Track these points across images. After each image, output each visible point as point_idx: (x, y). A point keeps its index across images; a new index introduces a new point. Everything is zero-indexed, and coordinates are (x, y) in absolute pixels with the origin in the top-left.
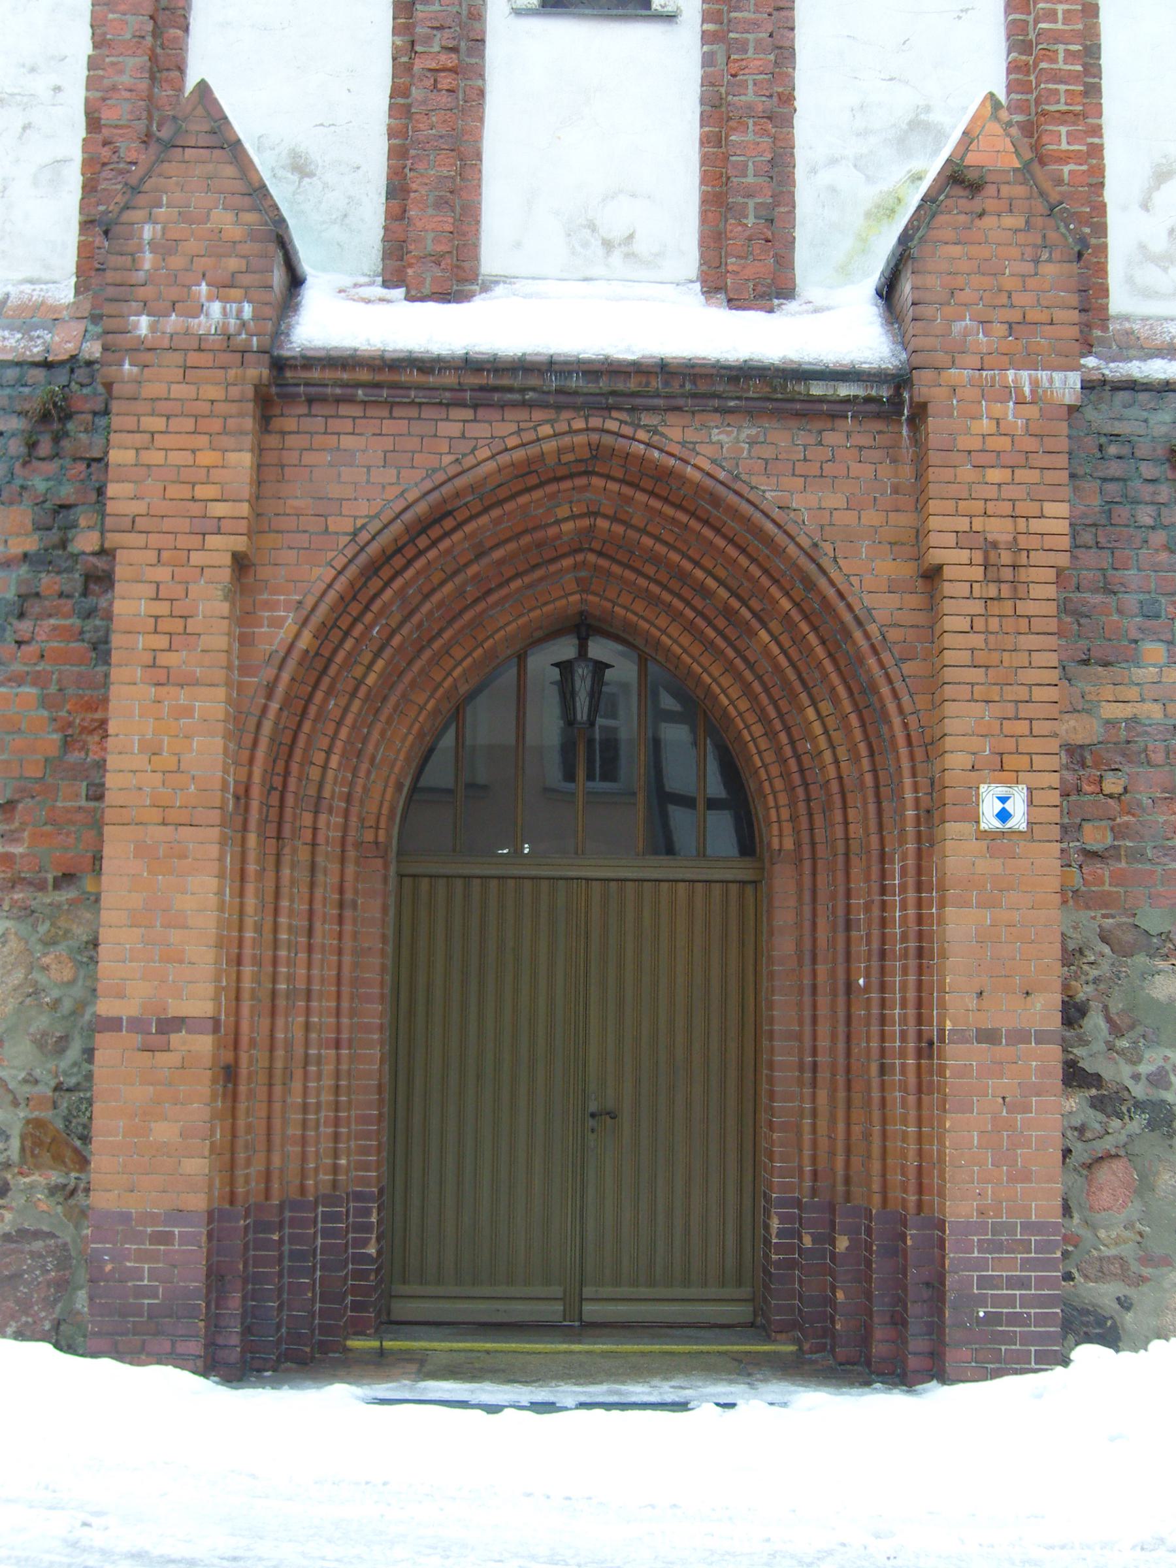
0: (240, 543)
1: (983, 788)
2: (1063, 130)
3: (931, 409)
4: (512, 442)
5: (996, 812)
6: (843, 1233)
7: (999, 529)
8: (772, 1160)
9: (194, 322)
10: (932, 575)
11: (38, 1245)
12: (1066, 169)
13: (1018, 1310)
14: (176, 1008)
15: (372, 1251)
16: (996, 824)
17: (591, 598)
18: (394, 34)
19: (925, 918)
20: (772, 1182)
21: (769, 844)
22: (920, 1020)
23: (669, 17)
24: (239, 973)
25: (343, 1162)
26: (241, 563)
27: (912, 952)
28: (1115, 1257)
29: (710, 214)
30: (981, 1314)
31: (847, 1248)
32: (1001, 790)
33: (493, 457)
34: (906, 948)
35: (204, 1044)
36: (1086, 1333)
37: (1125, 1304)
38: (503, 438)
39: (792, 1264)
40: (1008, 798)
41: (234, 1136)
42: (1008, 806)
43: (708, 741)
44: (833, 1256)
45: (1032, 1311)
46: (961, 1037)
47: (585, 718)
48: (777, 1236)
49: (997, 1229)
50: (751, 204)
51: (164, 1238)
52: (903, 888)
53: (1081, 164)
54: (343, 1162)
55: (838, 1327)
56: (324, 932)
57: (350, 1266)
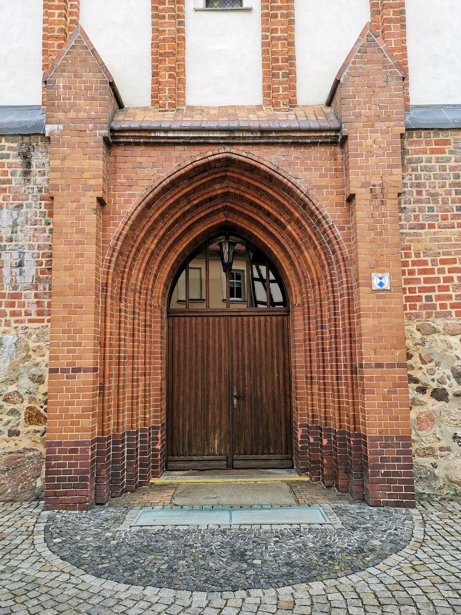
0: (100, 194)
1: (373, 274)
3: (349, 138)
6: (325, 438)
7: (376, 180)
8: (297, 411)
11: (31, 454)
13: (397, 470)
14: (79, 363)
18: (152, 18)
20: (297, 418)
21: (292, 302)
22: (351, 361)
23: (249, 10)
24: (104, 350)
26: (101, 202)
29: (266, 79)
30: (383, 472)
31: (327, 444)
32: (380, 275)
33: (191, 163)
34: (345, 334)
35: (90, 377)
36: (420, 477)
37: (435, 466)
38: (194, 157)
40: (383, 278)
42: (383, 281)
44: (321, 446)
45: (402, 471)
47: (227, 261)
49: (387, 438)
52: (343, 313)
53: (218, 451)
55: (325, 473)
56: (140, 336)
57: (151, 453)
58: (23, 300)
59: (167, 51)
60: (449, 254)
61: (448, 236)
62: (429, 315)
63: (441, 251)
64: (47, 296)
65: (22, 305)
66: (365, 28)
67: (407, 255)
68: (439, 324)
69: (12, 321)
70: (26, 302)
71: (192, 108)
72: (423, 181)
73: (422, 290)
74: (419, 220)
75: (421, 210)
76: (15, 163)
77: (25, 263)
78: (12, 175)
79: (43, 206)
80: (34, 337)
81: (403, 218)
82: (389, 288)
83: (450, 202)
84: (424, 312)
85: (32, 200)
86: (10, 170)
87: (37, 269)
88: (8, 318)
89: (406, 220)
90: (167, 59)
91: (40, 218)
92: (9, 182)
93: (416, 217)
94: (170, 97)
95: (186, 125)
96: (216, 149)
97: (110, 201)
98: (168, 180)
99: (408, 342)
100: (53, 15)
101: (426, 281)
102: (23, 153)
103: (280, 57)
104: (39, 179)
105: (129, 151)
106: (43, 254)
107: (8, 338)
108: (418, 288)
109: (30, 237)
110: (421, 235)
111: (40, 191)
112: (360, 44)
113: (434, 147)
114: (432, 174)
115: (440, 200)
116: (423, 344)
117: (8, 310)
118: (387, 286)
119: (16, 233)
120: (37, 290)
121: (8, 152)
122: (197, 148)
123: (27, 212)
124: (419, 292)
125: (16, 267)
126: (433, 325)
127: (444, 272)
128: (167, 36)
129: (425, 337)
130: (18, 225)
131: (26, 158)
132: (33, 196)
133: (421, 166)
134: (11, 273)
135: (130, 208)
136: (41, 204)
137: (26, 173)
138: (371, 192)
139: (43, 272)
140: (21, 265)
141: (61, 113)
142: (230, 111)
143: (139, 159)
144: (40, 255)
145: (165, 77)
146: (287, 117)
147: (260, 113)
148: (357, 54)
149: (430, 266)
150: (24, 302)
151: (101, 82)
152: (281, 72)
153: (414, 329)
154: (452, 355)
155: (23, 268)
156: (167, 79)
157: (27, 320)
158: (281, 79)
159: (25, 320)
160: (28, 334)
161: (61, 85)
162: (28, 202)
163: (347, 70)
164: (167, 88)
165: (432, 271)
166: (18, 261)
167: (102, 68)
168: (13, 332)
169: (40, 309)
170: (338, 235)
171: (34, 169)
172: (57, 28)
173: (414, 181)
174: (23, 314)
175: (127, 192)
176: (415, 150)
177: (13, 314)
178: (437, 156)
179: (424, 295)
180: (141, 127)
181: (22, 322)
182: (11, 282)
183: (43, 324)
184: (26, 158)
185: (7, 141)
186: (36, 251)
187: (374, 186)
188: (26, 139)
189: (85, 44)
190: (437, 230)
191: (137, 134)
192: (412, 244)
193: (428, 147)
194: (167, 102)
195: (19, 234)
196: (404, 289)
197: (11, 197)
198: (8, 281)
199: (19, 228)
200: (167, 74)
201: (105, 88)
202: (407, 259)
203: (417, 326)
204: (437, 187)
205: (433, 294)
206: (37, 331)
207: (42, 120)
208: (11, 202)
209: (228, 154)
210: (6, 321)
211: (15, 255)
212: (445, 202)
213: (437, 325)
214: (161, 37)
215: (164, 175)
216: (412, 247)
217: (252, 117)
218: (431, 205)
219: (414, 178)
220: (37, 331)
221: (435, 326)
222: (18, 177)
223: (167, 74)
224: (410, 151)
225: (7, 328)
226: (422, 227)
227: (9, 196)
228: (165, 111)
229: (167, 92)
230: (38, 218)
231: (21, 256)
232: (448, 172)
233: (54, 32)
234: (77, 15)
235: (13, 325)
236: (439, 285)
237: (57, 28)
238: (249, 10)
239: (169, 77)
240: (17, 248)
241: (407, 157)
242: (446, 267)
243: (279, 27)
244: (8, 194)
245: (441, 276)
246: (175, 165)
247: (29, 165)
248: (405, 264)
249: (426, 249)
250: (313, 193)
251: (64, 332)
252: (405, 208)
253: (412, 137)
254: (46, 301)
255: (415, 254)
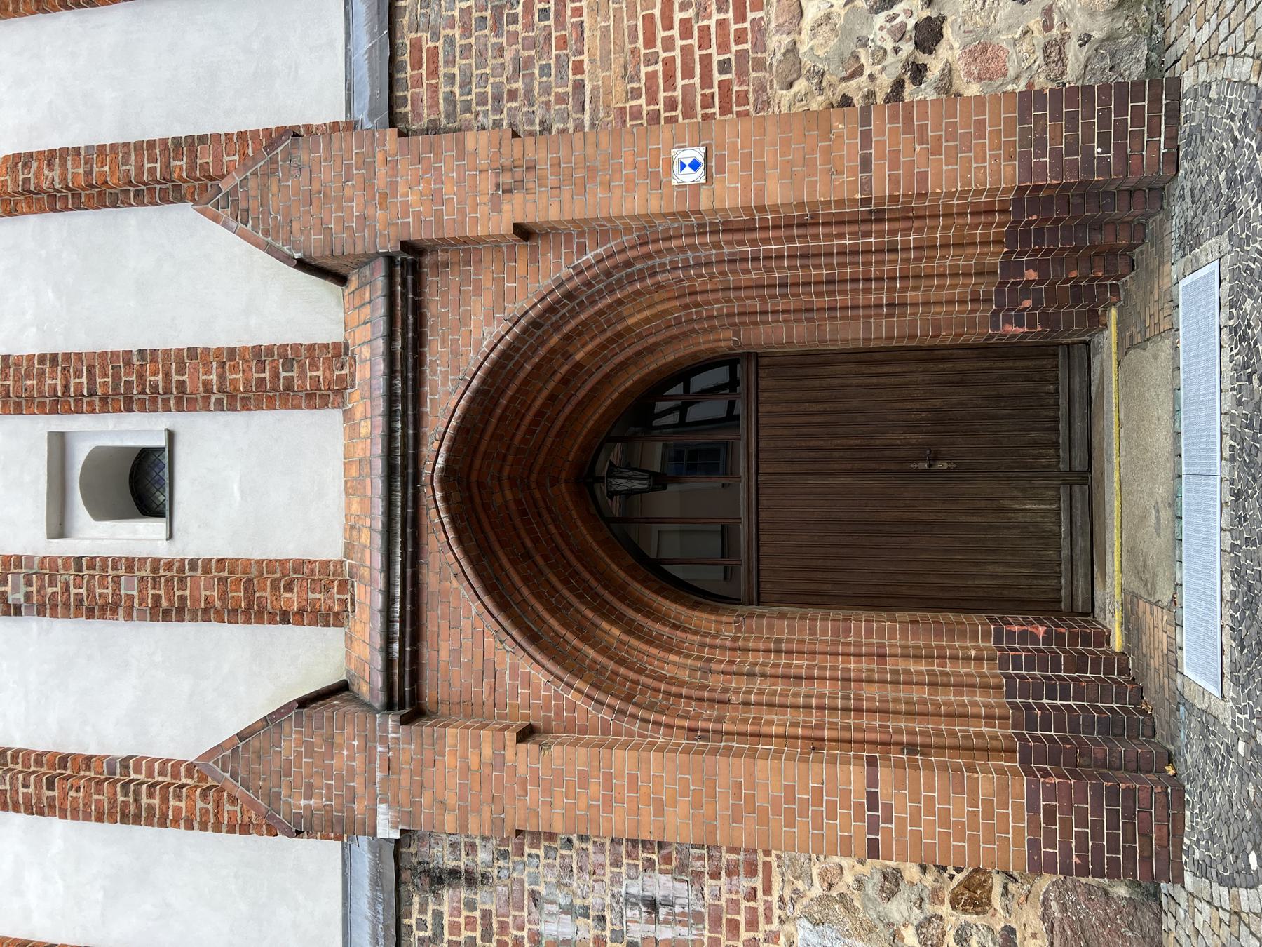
2: (226, 158)
3: (405, 238)
5: (692, 171)
9: (358, 770)
10: (523, 232)
14: (858, 793)
15: (1041, 629)
16: (701, 169)
17: (563, 475)
19: (775, 224)
23: (171, 435)
25: (973, 653)
27: (801, 231)
28: (1045, 51)
30: (1100, 150)
31: (1035, 271)
32: (676, 167)
39: (1044, 315)
41: (958, 748)
42: (687, 162)
43: (667, 393)
46: (865, 186)
48: (1021, 326)
49: (1025, 142)
51: (1050, 814)
52: (753, 242)
54: (973, 653)
56: (799, 664)
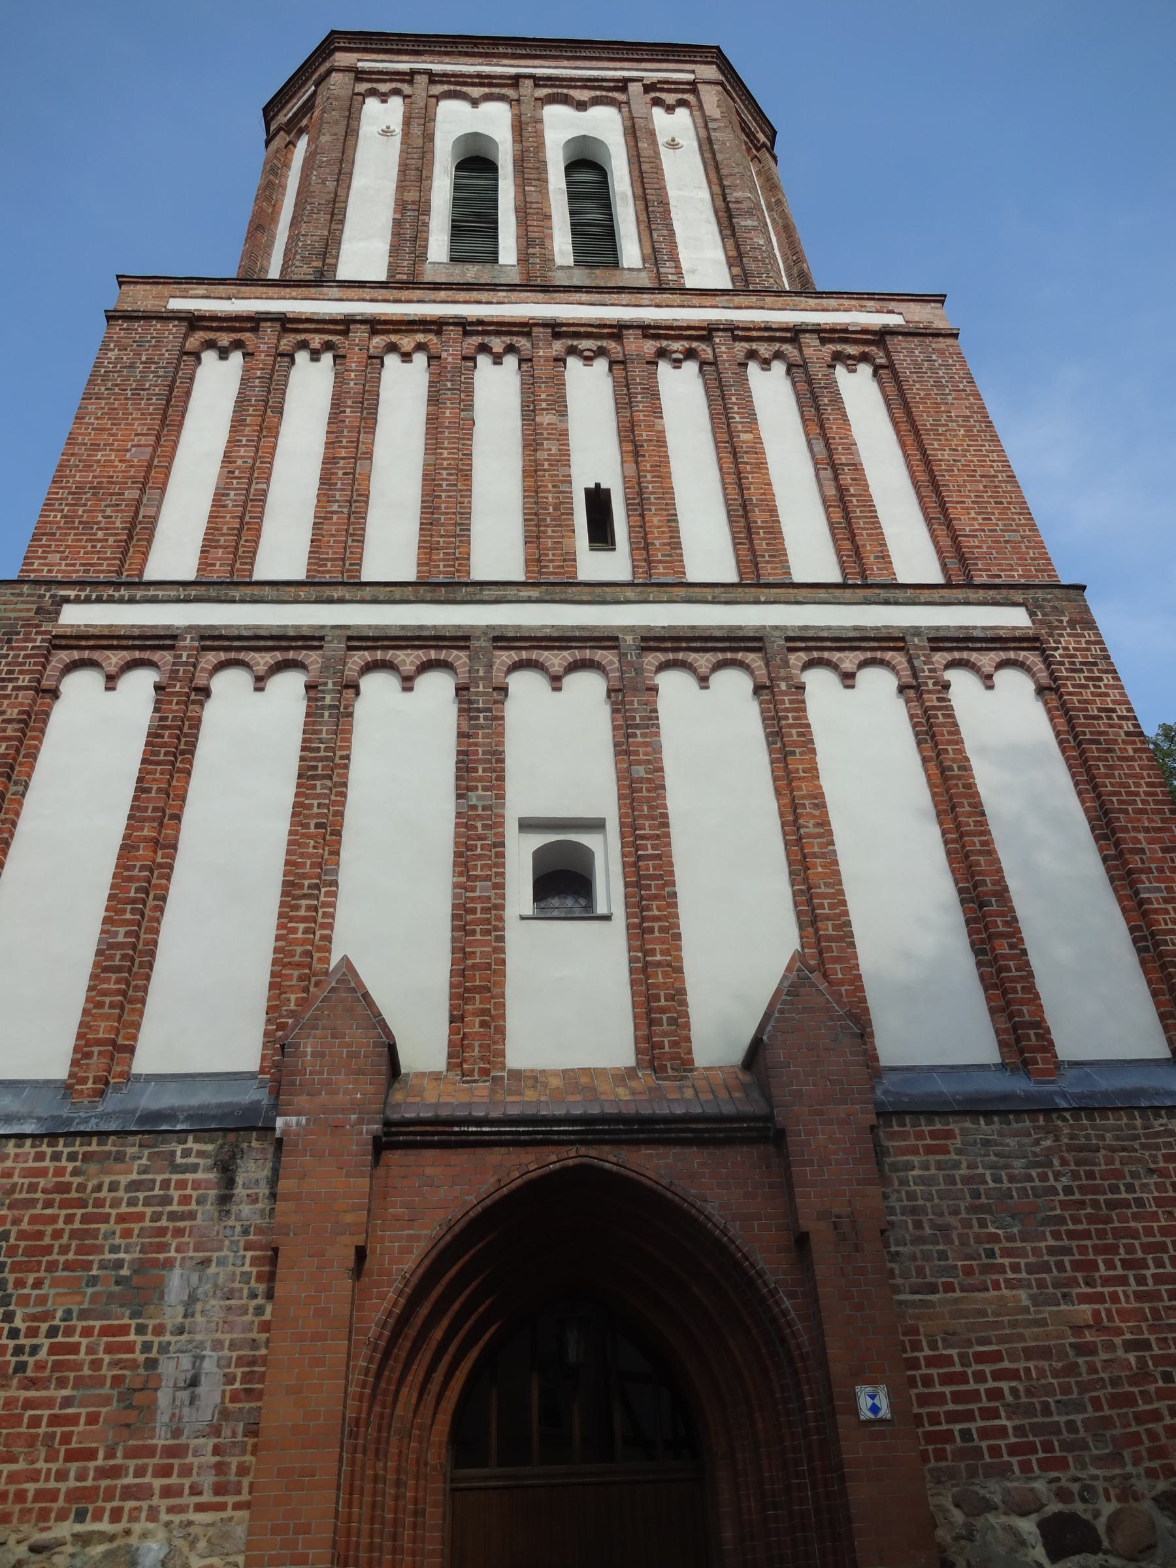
0: (360, 1240)
1: (858, 1389)
4: (532, 1167)
12: (843, 989)
16: (871, 1416)
23: (607, 918)
26: (361, 1254)
32: (869, 1389)
33: (521, 1176)
42: (876, 1401)
50: (665, 1017)
58: (190, 1459)
59: (477, 983)
60: (986, 1341)
61: (979, 1306)
62: (972, 1473)
63: (973, 1336)
64: (237, 1451)
65: (186, 1471)
66: (793, 959)
67: (916, 1346)
68: (993, 1490)
69: (163, 1509)
70: (196, 1464)
71: (516, 1075)
72: (920, 1202)
73: (953, 1417)
74: (925, 1277)
75: (926, 1256)
76: (207, 1181)
77: (203, 1378)
78: (198, 1203)
79: (248, 1261)
80: (202, 1545)
81: (897, 1272)
82: (889, 1416)
83: (972, 1241)
84: (962, 1465)
85: (230, 1249)
86: (195, 1194)
87: (224, 1392)
88: (156, 1501)
89: (905, 1275)
90: (477, 996)
91: (241, 1285)
92: (192, 1216)
93: (920, 1271)
94: (482, 1059)
95: (514, 1111)
96: (563, 1151)
97: (374, 1251)
98: (479, 1208)
99: (940, 1532)
100: (294, 931)
101: (957, 1397)
102: (221, 1161)
103: (662, 994)
104: (246, 1209)
105: (412, 1156)
106: (239, 1358)
107: (150, 1549)
108: (938, 1292)
109: (217, 1324)
110: (931, 1304)
111: (245, 1232)
112: (786, 984)
113: (929, 1142)
114: (934, 1189)
115: (955, 1237)
116: (970, 1538)
117: (158, 1483)
118: (885, 1412)
119: (193, 1316)
120: (219, 1437)
121: (196, 1160)
122: (530, 1149)
123: (218, 1274)
124: (947, 1422)
125: (185, 1389)
126: (982, 1492)
127: (985, 1381)
128: (478, 961)
129: (971, 1520)
130: (198, 1300)
131: (228, 1170)
132: (232, 1242)
133: (913, 1177)
134: (174, 1400)
135: (409, 1264)
136: (244, 1257)
137: (225, 1199)
138: (836, 1228)
139: (234, 1398)
140: (194, 1382)
141: (304, 1097)
142: (584, 1080)
143: (429, 1171)
144: (234, 1360)
145: (474, 1025)
146: (682, 1093)
147: (634, 1084)
148: (784, 997)
149: (958, 1368)
150: (192, 1464)
151: (376, 1045)
152: (665, 1017)
153: (948, 1503)
154: (1028, 1559)
155: (199, 1390)
156: (477, 1028)
157: (192, 1506)
158: (665, 1027)
159: (188, 1506)
160: (191, 1538)
161: (309, 1050)
162: (222, 1254)
163: (772, 1023)
164: (477, 1044)
165: (962, 1378)
166: (189, 1376)
167: (379, 1022)
168: (162, 1534)
169: (222, 1478)
170: (787, 1308)
171: (240, 1191)
172: (299, 949)
173: (906, 1203)
174: (187, 1491)
175: (406, 1232)
176: (899, 1147)
177: (167, 1492)
178: (938, 1157)
179: (957, 1427)
180: (437, 1116)
181: (181, 1509)
182: (171, 1420)
183: (224, 1515)
184: (228, 1170)
185: (195, 1141)
186: (226, 1353)
187: (838, 1217)
188: (232, 1137)
189: (353, 985)
190: (958, 1294)
191: (429, 1128)
192: (921, 1324)
193: (920, 1143)
194: (476, 1067)
195: (199, 1318)
196: (918, 1417)
197: (191, 1246)
198: (165, 1418)
199: (199, 1307)
200: (477, 1020)
201: (380, 1054)
202: (917, 1354)
203: (953, 1496)
204: (946, 1213)
205: (973, 1426)
206: (211, 1532)
207: (259, 1101)
208: (191, 1254)
209: (585, 1160)
210: (150, 1507)
211: (186, 1362)
212: (964, 1242)
213: (990, 1492)
214: (469, 962)
215: (472, 1199)
216: (922, 1330)
217: (623, 1093)
218: (940, 1247)
219: (904, 1198)
220: (211, 1532)
221: (988, 1496)
222: (208, 1207)
223: (477, 1020)
224: (891, 1150)
225: (151, 1526)
226: (933, 1289)
227: (188, 1243)
228: (474, 1081)
229: (477, 1050)
230: (237, 1285)
231: (197, 1364)
232: (959, 1186)
233: (294, 956)
234: (331, 926)
235: (164, 1517)
236: (979, 1405)
237: (299, 949)
238: (607, 918)
239: (481, 1026)
240: (190, 1347)
241: (889, 1160)
242: (987, 1369)
243: (658, 947)
244: (186, 1239)
245: (982, 1388)
246: (492, 1180)
247: (230, 1183)
248: (914, 1364)
249: (946, 1333)
250: (734, 1229)
251: (275, 1530)
252: (898, 1253)
253: (892, 1126)
254: (234, 1461)
255: (928, 1342)
